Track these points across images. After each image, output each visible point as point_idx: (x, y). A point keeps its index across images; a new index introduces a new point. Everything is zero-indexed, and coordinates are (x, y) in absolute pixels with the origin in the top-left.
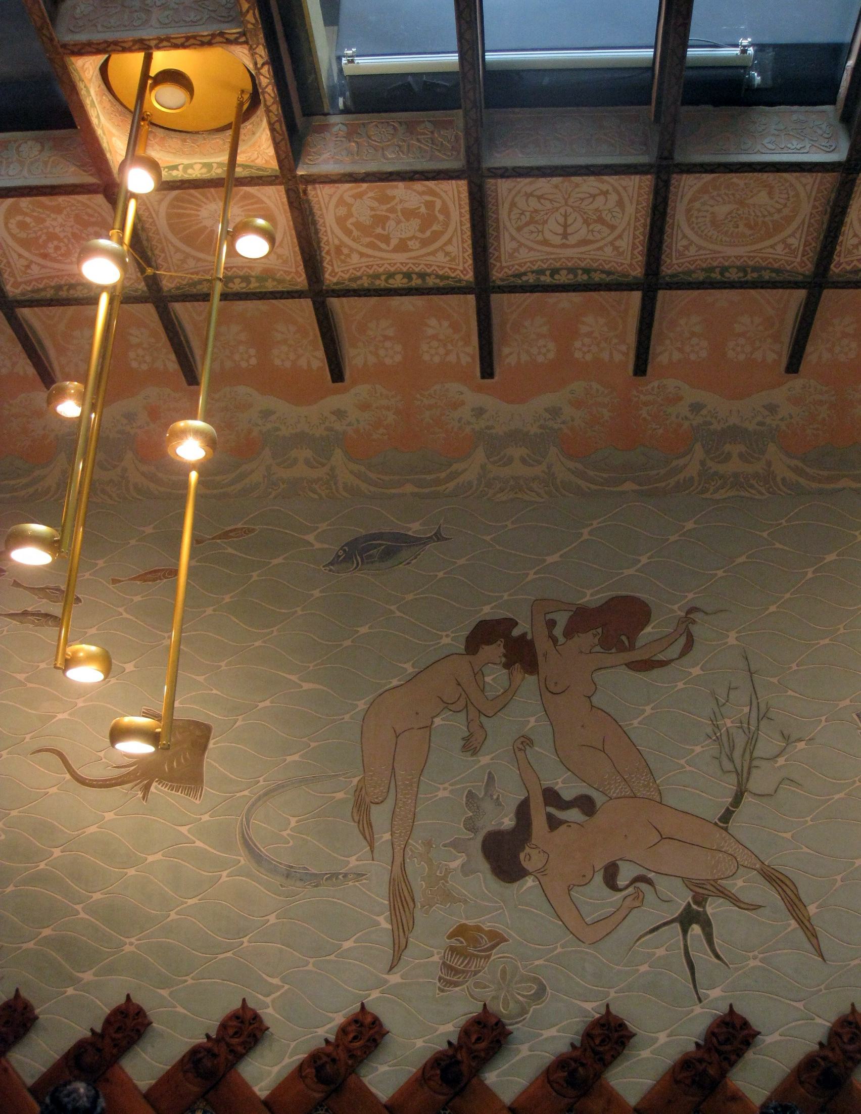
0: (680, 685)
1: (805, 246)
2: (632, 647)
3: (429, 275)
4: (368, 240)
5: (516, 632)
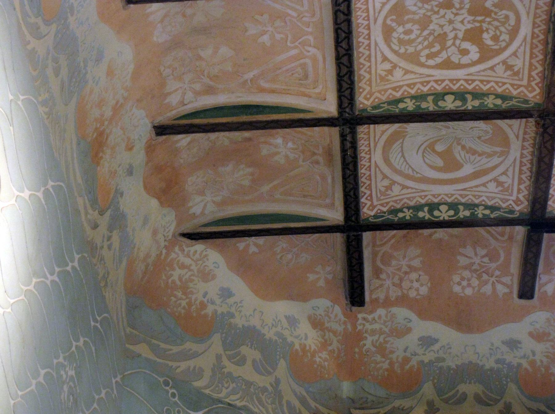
3: (477, 206)
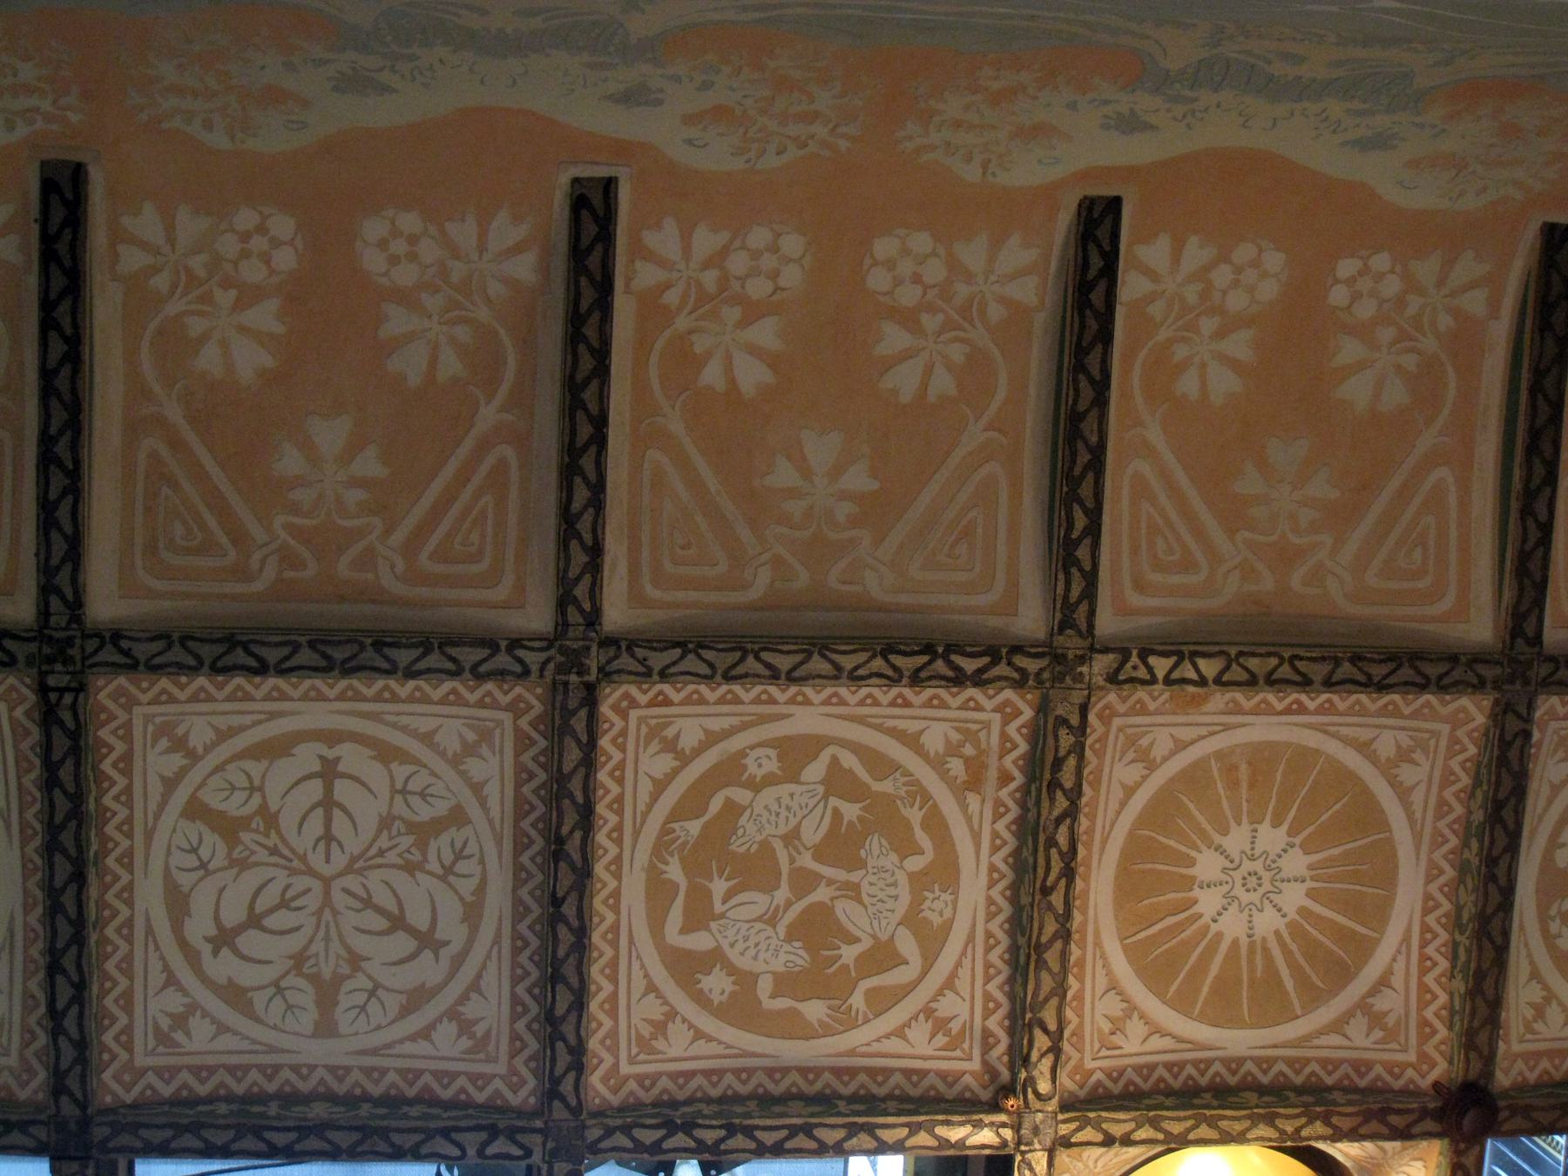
4: (886, 786)
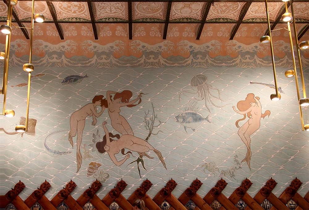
0: (138, 110)
1: (164, 14)
2: (128, 102)
3: (81, 19)
4: (67, 11)
5: (103, 98)
